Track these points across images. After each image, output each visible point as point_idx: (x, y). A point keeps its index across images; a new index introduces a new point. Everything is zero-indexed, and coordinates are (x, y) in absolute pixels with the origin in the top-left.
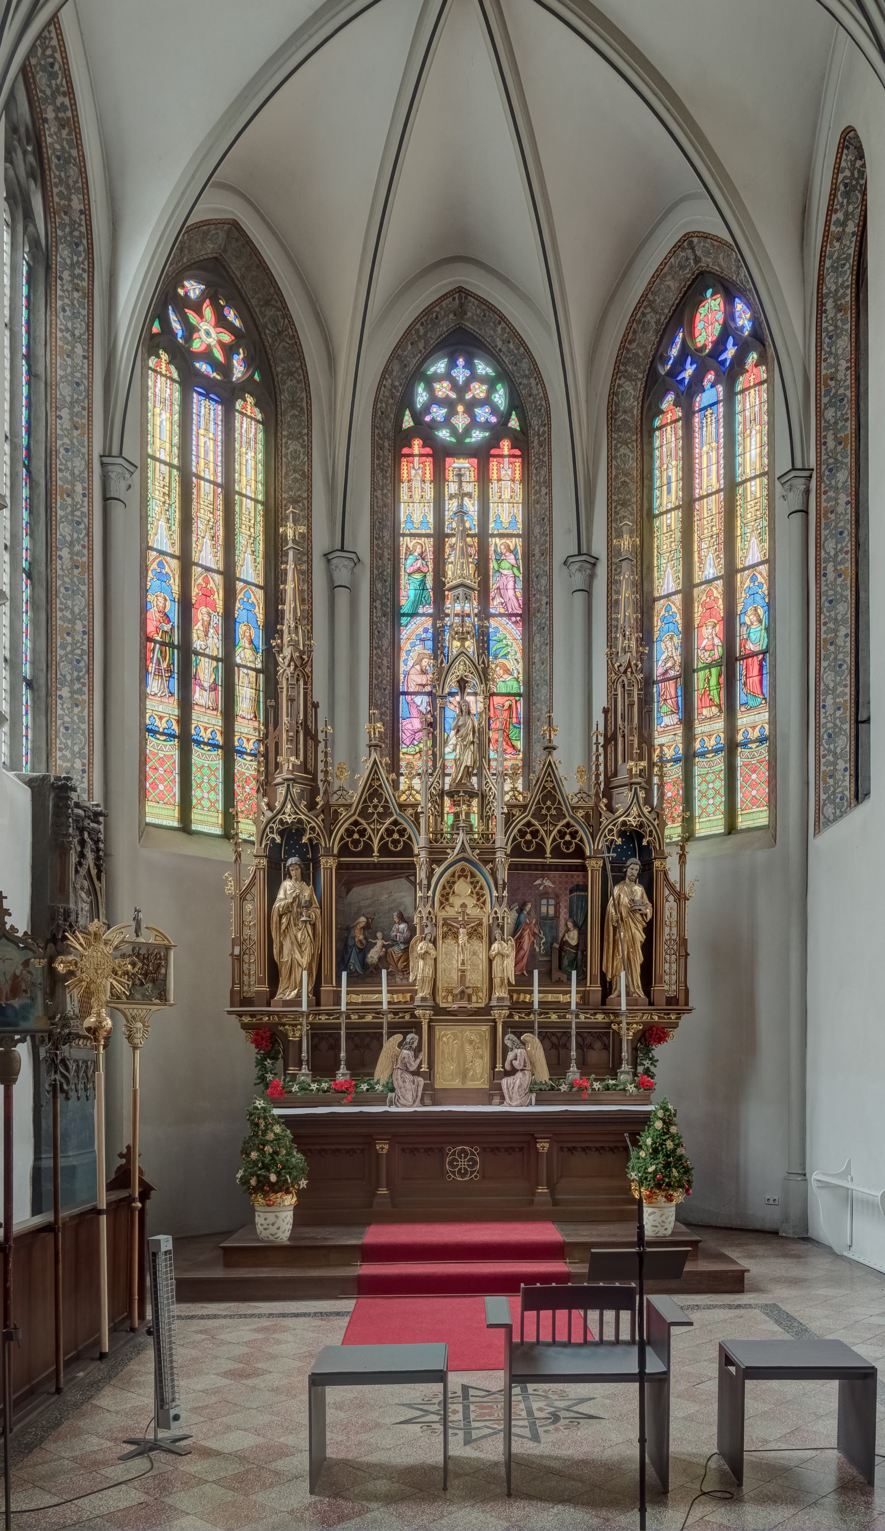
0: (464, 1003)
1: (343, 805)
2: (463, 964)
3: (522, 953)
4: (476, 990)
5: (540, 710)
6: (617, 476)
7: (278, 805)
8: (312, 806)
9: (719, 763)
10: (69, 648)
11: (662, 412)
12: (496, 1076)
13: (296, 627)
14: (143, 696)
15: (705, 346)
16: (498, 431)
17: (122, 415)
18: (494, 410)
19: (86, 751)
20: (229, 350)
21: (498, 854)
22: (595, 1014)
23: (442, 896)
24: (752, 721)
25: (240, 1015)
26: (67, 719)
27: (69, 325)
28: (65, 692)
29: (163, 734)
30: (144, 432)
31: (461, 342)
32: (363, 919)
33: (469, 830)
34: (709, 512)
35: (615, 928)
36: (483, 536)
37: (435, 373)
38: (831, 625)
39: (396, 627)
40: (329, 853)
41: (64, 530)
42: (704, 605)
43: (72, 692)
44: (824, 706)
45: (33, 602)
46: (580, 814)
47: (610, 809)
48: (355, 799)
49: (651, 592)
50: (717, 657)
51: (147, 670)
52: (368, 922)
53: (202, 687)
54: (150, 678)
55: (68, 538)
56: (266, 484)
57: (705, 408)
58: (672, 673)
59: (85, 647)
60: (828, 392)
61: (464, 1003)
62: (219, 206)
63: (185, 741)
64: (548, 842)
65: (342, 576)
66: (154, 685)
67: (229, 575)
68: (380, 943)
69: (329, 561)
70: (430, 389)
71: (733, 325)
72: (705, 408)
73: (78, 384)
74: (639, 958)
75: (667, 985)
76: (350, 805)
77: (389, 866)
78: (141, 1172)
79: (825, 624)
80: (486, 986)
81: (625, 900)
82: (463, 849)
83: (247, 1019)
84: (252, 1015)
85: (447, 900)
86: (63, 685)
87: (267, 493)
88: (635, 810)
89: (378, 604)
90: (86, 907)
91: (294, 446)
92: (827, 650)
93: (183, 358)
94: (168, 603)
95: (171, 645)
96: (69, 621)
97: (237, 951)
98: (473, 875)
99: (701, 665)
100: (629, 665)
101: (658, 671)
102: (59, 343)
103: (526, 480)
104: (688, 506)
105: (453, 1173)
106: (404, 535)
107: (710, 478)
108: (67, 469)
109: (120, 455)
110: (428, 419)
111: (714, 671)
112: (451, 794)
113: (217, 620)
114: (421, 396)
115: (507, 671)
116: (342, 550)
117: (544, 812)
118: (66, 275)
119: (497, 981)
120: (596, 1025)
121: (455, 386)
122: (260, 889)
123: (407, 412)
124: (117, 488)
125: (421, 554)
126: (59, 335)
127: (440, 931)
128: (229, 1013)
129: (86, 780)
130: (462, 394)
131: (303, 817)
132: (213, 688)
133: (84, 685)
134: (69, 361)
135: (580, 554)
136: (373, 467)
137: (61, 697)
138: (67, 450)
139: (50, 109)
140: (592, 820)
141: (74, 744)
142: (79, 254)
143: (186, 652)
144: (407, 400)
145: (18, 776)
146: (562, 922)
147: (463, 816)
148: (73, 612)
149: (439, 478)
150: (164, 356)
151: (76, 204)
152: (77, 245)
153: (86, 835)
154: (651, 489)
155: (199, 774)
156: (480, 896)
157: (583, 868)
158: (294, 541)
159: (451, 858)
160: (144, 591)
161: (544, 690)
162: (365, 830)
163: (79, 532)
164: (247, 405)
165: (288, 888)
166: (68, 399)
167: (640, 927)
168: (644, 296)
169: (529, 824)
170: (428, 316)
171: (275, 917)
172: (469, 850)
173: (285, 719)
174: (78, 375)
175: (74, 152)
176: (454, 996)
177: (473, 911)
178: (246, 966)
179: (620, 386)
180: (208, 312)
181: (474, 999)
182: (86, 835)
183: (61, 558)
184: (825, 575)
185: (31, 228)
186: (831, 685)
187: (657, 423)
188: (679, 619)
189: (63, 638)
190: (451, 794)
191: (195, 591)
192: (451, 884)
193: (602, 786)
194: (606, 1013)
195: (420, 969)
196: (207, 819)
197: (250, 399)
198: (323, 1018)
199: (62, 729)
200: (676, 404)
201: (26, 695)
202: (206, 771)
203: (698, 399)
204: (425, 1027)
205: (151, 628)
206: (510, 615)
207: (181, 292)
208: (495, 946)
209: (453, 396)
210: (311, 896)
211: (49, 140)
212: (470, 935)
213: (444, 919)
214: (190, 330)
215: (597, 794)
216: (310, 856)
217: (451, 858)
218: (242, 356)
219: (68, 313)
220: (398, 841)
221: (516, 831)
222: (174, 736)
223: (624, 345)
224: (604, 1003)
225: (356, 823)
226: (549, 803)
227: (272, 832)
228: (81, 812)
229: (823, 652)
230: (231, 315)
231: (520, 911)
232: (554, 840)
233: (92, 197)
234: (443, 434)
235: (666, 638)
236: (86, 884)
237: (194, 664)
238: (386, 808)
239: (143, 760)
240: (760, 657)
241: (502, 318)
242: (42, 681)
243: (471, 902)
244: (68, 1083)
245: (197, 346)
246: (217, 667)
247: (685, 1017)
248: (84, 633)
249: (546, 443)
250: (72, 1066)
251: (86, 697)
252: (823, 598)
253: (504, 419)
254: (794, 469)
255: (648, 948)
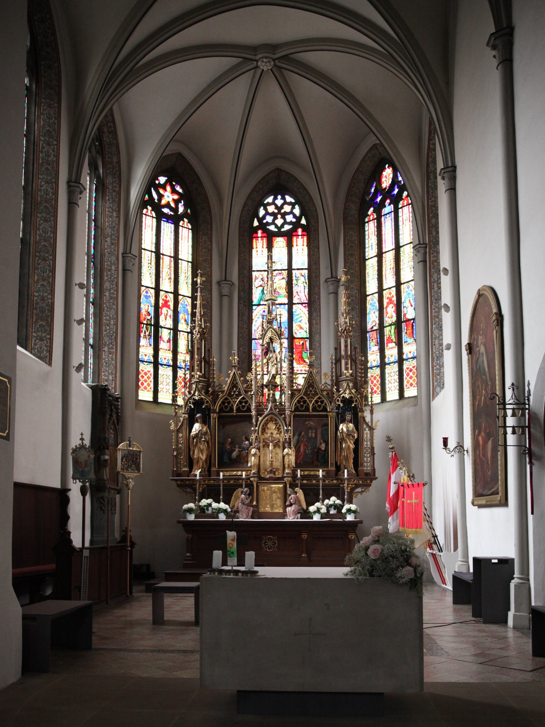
0: (272, 475)
1: (221, 391)
2: (272, 458)
3: (300, 454)
4: (277, 469)
5: (316, 345)
6: (348, 244)
7: (192, 392)
8: (207, 392)
9: (396, 367)
10: (108, 331)
11: (368, 215)
12: (285, 507)
13: (201, 319)
14: (138, 346)
15: (386, 188)
16: (296, 225)
17: (133, 233)
18: (295, 216)
19: (114, 372)
20: (177, 202)
21: (287, 412)
22: (332, 480)
23: (262, 429)
24: (410, 349)
25: (176, 480)
26: (107, 359)
27: (111, 205)
28: (106, 349)
29: (146, 362)
30: (140, 240)
31: (279, 190)
32: (230, 440)
33: (275, 400)
34: (389, 259)
35: (341, 443)
36: (290, 269)
37: (268, 202)
38: (437, 310)
39: (251, 311)
40: (214, 412)
41: (107, 285)
42: (388, 298)
43: (109, 348)
44: (435, 345)
45: (95, 314)
46: (325, 393)
47: (338, 391)
48: (226, 389)
49: (365, 291)
50: (394, 321)
51: (140, 336)
52: (232, 441)
53: (163, 341)
54: (142, 339)
55: (109, 288)
56: (193, 255)
57: (386, 214)
58: (375, 328)
59: (114, 330)
60: (432, 212)
61: (272, 475)
62: (174, 148)
63: (156, 364)
64: (311, 405)
65: (225, 291)
66: (143, 342)
67: (176, 293)
68: (237, 450)
69: (220, 285)
70: (265, 209)
71: (396, 180)
72: (386, 214)
73: (114, 228)
74: (352, 455)
75: (367, 467)
76: (224, 391)
77: (241, 416)
78: (131, 537)
79: (434, 309)
80: (281, 468)
81: (345, 430)
82: (271, 409)
83: (179, 483)
84: (182, 480)
85: (265, 431)
86: (105, 346)
87: (193, 258)
88: (348, 391)
89: (242, 302)
90: (112, 436)
91: (204, 238)
92: (435, 320)
93: (157, 208)
94: (150, 307)
95: (151, 325)
96: (110, 212)
97: (175, 453)
98: (276, 420)
99: (387, 325)
100: (345, 329)
101: (369, 327)
102: (107, 213)
103: (309, 245)
104: (380, 255)
105: (266, 547)
106: (254, 271)
107: (389, 244)
108: (109, 261)
109: (130, 253)
110: (265, 221)
111: (393, 327)
112: (267, 386)
113: (171, 313)
114: (262, 212)
115: (301, 328)
116: (225, 280)
117: (308, 392)
118: (110, 187)
119: (286, 466)
120: (334, 485)
121: (276, 207)
122: (185, 427)
123: (256, 219)
124: (129, 266)
125: (262, 279)
126: (107, 210)
127: (261, 445)
128: (172, 480)
129: (114, 384)
130: (280, 210)
131: (203, 397)
132: (169, 341)
133: (113, 345)
134: (111, 219)
135: (332, 277)
136: (239, 244)
137: (104, 351)
138: (109, 254)
139: (105, 128)
140: (330, 395)
141: (109, 370)
142: (115, 178)
143: (157, 326)
144: (256, 214)
145: (88, 385)
146: (318, 440)
147: (271, 396)
148: (110, 317)
149: (270, 247)
150: (150, 208)
151: (115, 160)
152: (115, 175)
153: (113, 407)
154: (365, 248)
155: (162, 378)
156: (279, 429)
157: (327, 416)
158: (201, 284)
159: (266, 413)
160: (139, 304)
161: (317, 336)
162: (230, 401)
163: (113, 285)
164: (185, 223)
165: (197, 427)
166: (110, 234)
167: (352, 442)
168: (358, 169)
169: (302, 398)
170: (263, 181)
171: (191, 440)
172: (273, 409)
173: (196, 356)
174: (114, 224)
175: (114, 142)
176: (268, 472)
177: (276, 435)
178: (179, 460)
179: (349, 206)
180: (168, 188)
181: (277, 473)
182: (113, 407)
183: (105, 296)
184: (433, 288)
185: (97, 172)
186: (437, 335)
187: (366, 220)
188: (377, 304)
189: (105, 327)
190: (267, 386)
191: (161, 302)
192: (266, 424)
193: (335, 381)
194: (337, 479)
195: (253, 460)
196: (165, 397)
197: (186, 220)
198: (212, 482)
199: (105, 364)
200: (374, 212)
201: (91, 351)
202: (165, 377)
203: (368, 335)
204: (255, 486)
205: (142, 318)
206: (302, 304)
207: (157, 182)
208: (286, 450)
209: (276, 211)
210: (207, 430)
211: (105, 139)
212: (275, 446)
213: (263, 439)
214: (161, 196)
215: (332, 384)
216: (207, 413)
217: (266, 413)
218: (183, 203)
219: (111, 201)
220: (245, 406)
221: (296, 401)
222: (151, 363)
223: (350, 188)
224: (336, 475)
225: (226, 399)
226: (311, 389)
227: (190, 403)
228: (111, 398)
229: (433, 321)
230: (178, 189)
231: (299, 435)
232: (313, 404)
233: (121, 157)
234: (272, 228)
235: (372, 312)
236: (112, 426)
237: (160, 332)
238: (239, 392)
239: (138, 373)
240: (412, 321)
241: (296, 179)
242: (97, 345)
243: (275, 432)
244: (104, 507)
245: (163, 202)
246: (170, 333)
247: (374, 482)
248: (114, 324)
249: (317, 230)
250: (106, 500)
251: (114, 350)
252: (433, 298)
253: (299, 219)
254: (419, 244)
255: (356, 451)
